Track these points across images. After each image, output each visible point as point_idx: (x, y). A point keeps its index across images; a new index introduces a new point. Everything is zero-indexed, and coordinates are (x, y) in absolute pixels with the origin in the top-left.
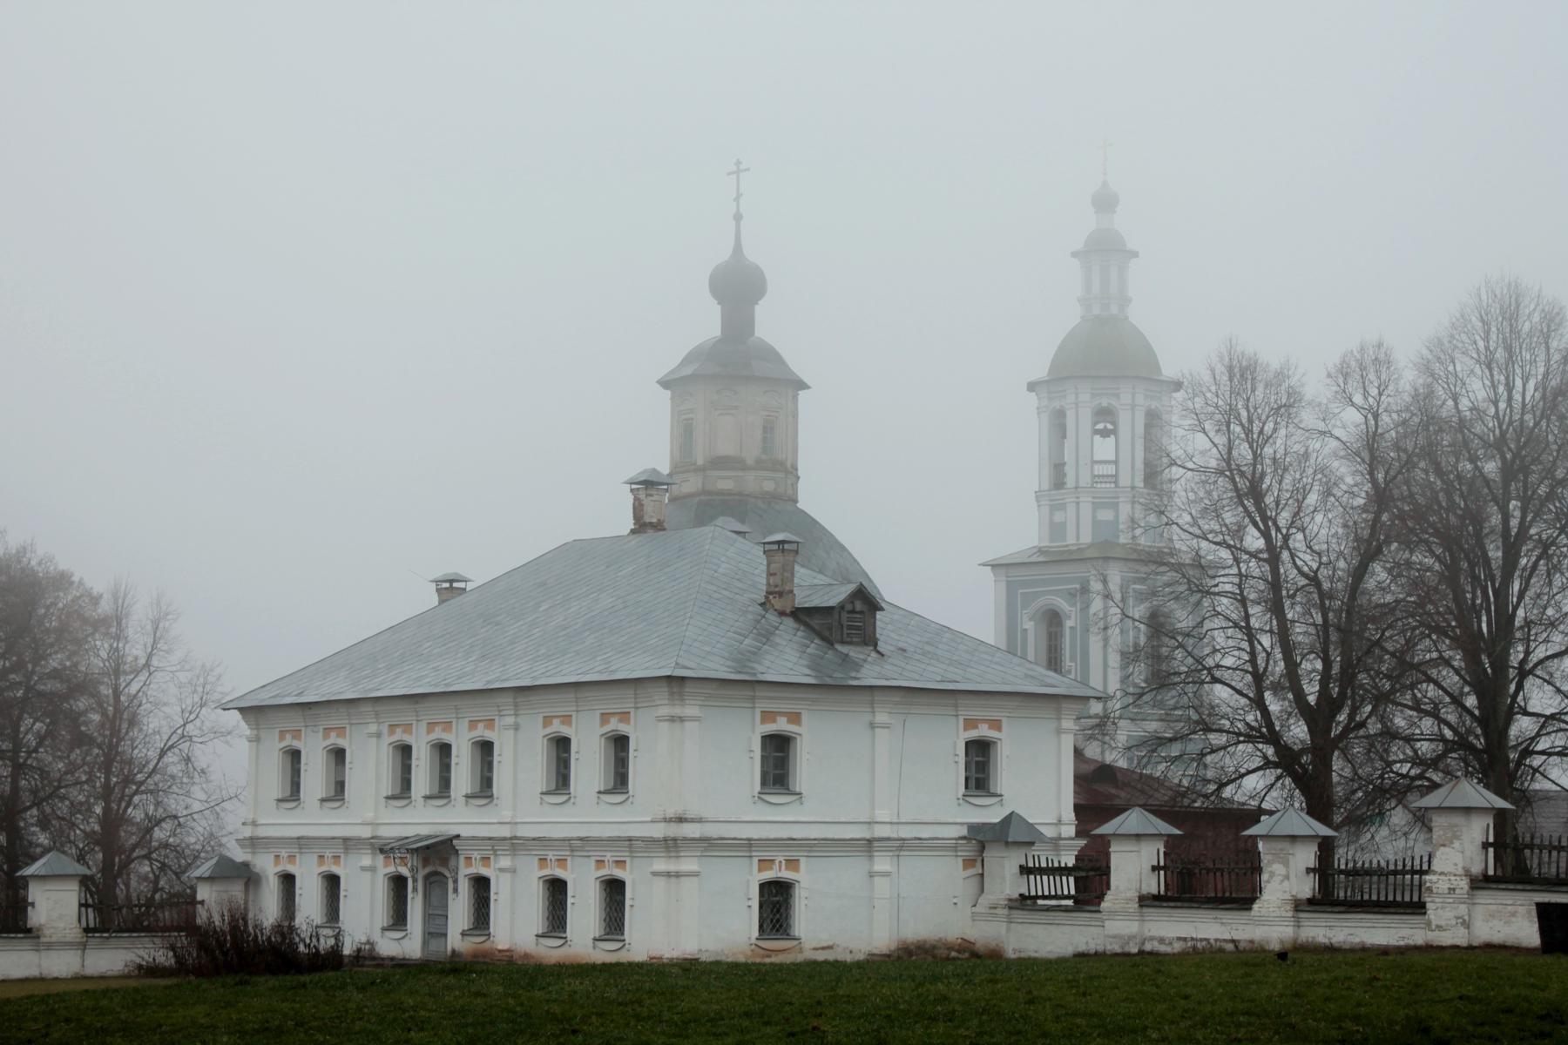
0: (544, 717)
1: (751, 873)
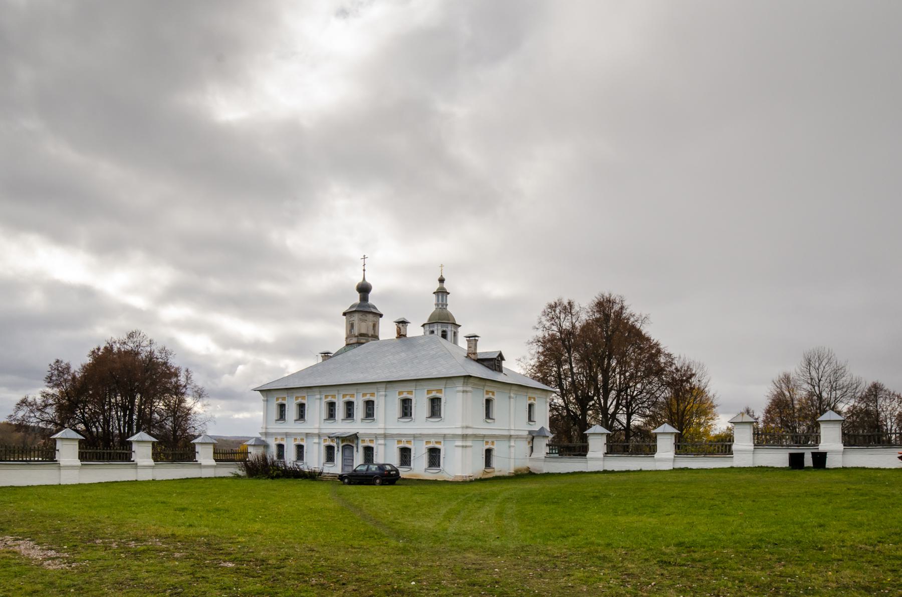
0: (399, 392)
1: (483, 446)
